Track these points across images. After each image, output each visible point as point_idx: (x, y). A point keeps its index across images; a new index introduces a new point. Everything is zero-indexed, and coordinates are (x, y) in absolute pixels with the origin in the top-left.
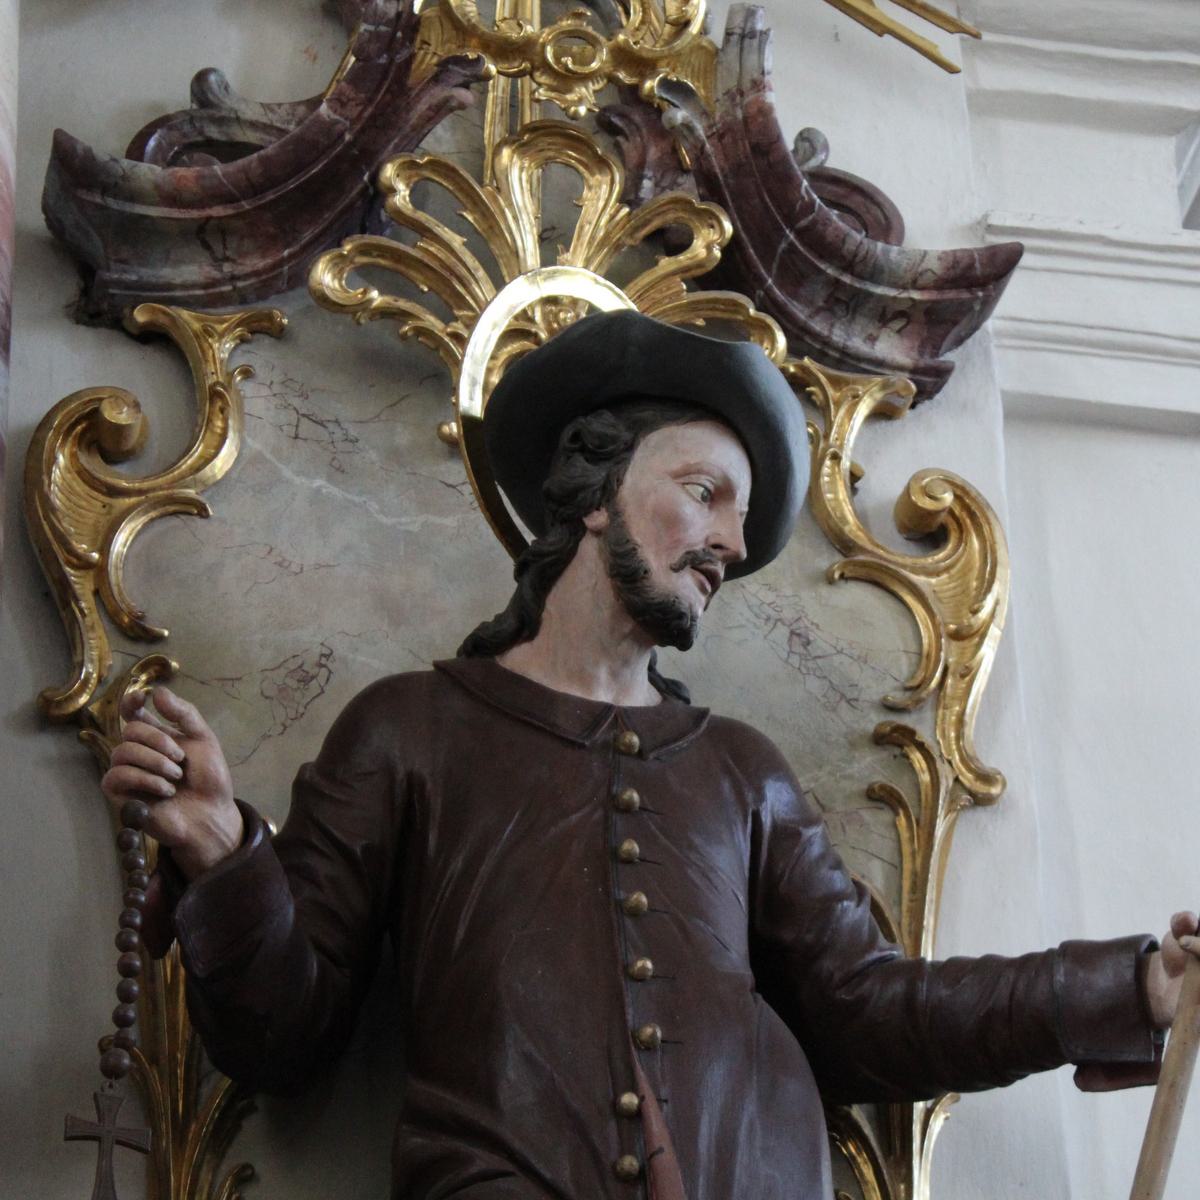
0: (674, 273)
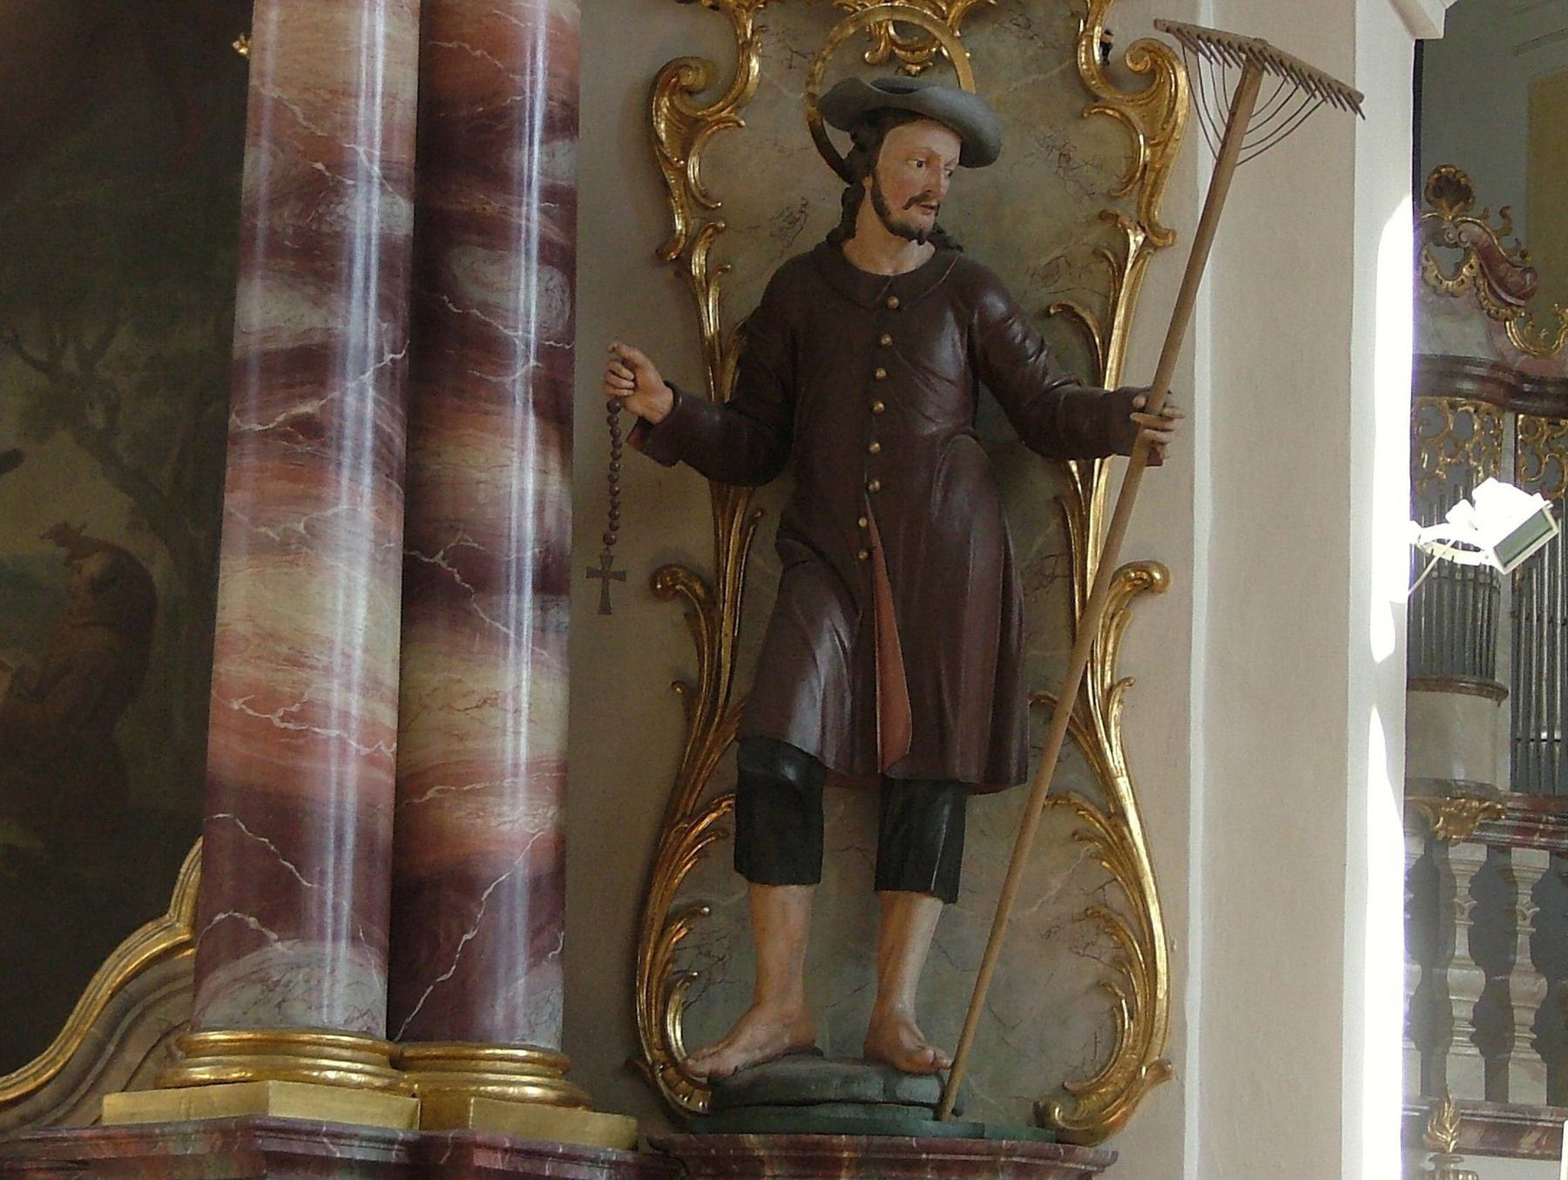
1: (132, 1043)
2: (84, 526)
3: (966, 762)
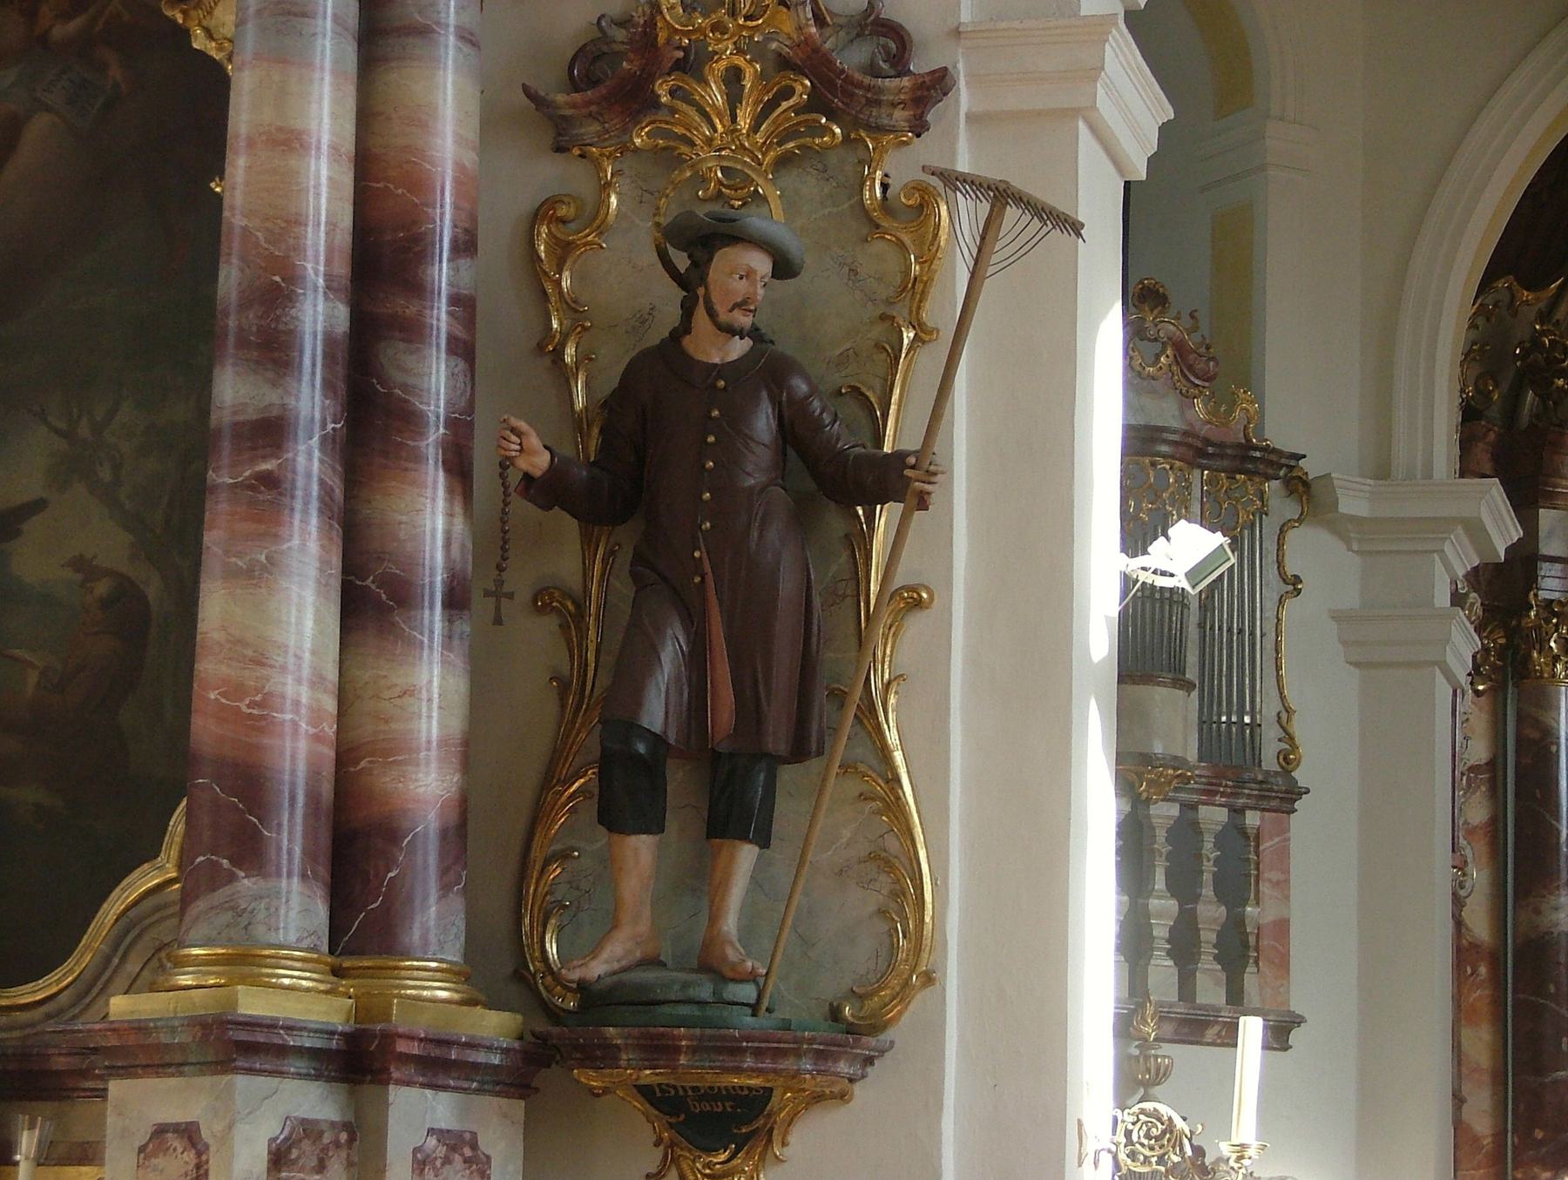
0: (789, 108)
1: (132, 956)
2: (95, 557)
3: (777, 739)
